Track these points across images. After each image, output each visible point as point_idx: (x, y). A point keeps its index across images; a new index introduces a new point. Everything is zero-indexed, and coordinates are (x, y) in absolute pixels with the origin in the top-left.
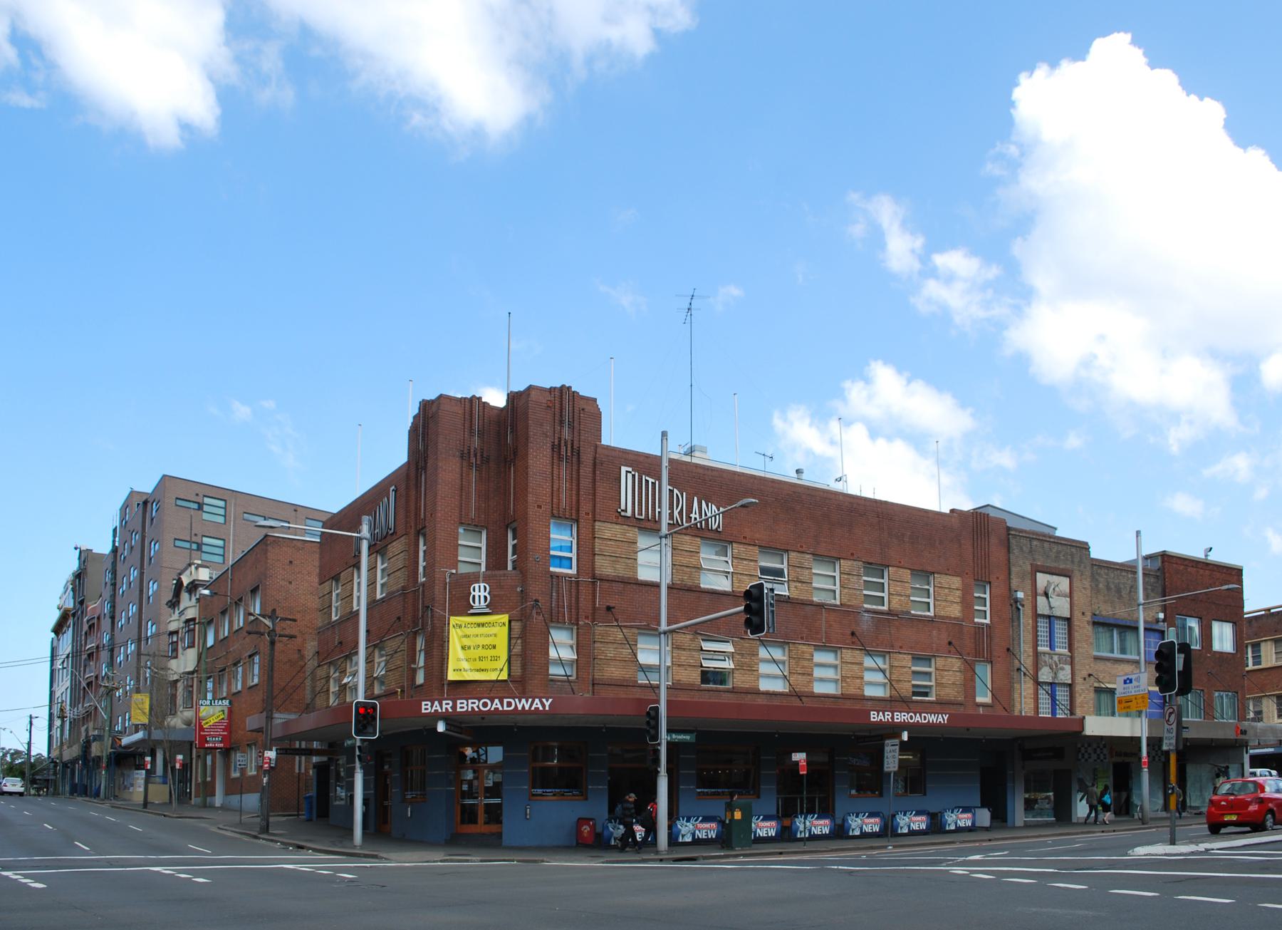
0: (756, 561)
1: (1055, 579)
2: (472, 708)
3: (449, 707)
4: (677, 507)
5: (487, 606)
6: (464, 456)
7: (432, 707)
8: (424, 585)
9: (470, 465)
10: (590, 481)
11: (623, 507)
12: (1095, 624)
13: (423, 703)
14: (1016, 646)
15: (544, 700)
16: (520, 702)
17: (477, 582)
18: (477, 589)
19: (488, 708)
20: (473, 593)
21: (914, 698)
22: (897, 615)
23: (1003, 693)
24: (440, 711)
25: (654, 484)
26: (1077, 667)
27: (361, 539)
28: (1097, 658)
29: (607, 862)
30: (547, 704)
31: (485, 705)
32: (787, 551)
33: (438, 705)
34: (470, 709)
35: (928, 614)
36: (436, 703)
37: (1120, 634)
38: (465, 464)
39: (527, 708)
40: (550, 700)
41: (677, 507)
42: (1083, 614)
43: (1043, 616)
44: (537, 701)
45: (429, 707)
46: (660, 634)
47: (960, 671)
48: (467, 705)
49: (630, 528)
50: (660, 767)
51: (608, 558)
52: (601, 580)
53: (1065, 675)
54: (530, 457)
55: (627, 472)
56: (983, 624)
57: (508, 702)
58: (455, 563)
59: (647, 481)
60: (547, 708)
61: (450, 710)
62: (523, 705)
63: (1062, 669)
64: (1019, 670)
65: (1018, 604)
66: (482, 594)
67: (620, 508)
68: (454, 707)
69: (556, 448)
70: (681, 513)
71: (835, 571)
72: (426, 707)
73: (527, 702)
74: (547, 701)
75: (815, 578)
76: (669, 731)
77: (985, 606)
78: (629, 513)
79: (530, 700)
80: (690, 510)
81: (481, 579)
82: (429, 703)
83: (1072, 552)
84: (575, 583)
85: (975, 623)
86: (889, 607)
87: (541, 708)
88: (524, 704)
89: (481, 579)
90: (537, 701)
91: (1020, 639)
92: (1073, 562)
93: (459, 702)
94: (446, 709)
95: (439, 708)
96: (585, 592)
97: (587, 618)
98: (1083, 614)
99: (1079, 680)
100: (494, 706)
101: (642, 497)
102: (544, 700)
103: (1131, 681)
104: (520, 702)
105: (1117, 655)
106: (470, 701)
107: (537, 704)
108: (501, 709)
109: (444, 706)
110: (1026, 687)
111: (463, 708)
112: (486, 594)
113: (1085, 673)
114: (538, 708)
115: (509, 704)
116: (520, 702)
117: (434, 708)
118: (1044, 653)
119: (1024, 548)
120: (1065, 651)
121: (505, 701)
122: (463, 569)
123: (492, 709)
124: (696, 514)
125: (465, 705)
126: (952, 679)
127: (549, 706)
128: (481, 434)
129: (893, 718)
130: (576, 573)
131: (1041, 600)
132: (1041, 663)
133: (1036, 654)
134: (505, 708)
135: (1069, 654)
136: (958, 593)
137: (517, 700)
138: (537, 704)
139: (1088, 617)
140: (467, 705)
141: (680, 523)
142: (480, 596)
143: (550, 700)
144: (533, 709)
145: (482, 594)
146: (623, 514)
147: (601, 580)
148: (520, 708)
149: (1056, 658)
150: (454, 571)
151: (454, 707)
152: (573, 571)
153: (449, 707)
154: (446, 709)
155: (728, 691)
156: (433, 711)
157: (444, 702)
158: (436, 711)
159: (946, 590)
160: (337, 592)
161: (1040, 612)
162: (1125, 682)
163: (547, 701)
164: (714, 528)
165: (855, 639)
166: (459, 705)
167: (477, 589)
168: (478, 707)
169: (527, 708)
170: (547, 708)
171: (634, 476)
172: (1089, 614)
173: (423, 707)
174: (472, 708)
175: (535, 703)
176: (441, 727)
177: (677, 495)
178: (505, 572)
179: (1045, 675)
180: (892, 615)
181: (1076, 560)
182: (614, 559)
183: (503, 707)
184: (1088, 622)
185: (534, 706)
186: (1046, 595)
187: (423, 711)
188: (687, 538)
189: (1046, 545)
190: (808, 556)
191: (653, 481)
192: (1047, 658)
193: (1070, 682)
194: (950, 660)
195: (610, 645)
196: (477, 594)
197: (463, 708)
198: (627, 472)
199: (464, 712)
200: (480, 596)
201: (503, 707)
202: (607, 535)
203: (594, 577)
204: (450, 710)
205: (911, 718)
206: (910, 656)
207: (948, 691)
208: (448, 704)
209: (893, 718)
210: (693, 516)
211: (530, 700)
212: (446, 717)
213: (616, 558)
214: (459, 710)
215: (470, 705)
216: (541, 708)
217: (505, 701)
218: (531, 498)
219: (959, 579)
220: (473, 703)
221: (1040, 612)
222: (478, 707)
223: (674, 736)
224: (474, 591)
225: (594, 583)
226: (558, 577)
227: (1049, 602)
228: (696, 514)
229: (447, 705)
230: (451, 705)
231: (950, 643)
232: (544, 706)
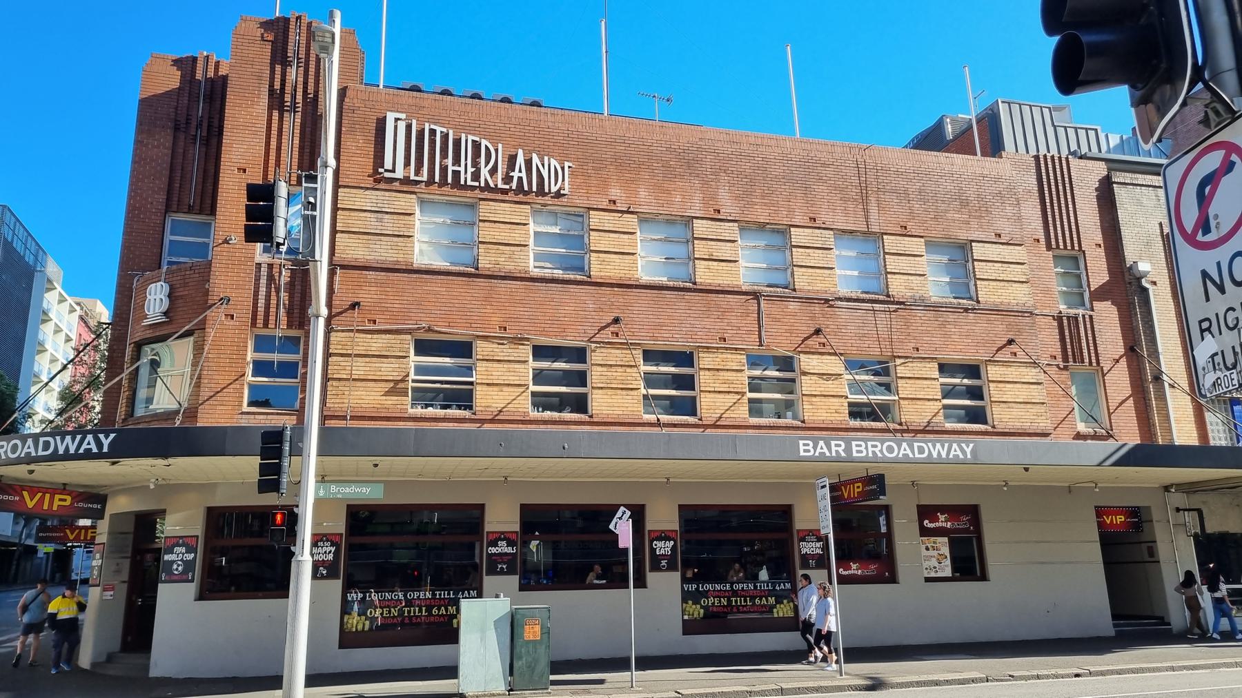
2: (874, 452)
3: (840, 449)
4: (487, 163)
7: (815, 448)
10: (1125, 239)
15: (101, 436)
16: (62, 442)
19: (894, 455)
30: (968, 451)
33: (32, 446)
36: (821, 443)
39: (944, 455)
41: (487, 163)
44: (90, 437)
45: (810, 448)
48: (866, 448)
50: (295, 545)
57: (44, 441)
59: (433, 132)
60: (969, 456)
61: (843, 454)
62: (939, 452)
65: (1143, 280)
67: (383, 167)
68: (848, 449)
73: (73, 440)
74: (107, 437)
79: (946, 445)
94: (837, 451)
95: (825, 450)
101: (435, 154)
102: (101, 436)
104: (62, 442)
106: (870, 444)
107: (89, 444)
108: (911, 456)
109: (834, 449)
114: (91, 449)
115: (921, 451)
116: (934, 447)
117: (819, 450)
124: (520, 171)
125: (863, 448)
127: (110, 445)
134: (917, 455)
138: (89, 444)
140: (866, 448)
141: (526, 188)
144: (951, 456)
145: (158, 297)
148: (935, 455)
151: (848, 449)
153: (840, 449)
156: (817, 454)
158: (822, 454)
163: (107, 437)
164: (554, 189)
166: (854, 449)
168: (881, 451)
169: (944, 455)
170: (969, 456)
171: (409, 127)
173: (802, 448)
174: (874, 452)
175: (953, 449)
177: (487, 147)
183: (914, 455)
185: (952, 453)
191: (445, 130)
197: (809, 451)
198: (397, 120)
199: (923, 458)
204: (843, 454)
208: (840, 446)
211: (946, 445)
215: (870, 449)
216: (961, 456)
220: (873, 446)
222: (881, 451)
224: (150, 295)
228: (520, 171)
230: (843, 446)
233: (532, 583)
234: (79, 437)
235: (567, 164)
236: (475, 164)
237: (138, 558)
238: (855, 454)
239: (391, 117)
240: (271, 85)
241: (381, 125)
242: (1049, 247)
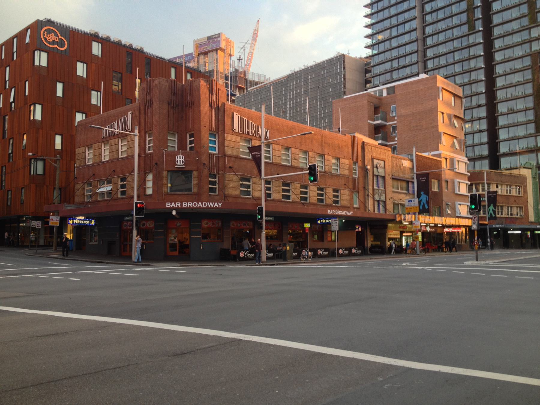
0: (280, 151)
1: (380, 162)
2: (189, 206)
5: (183, 165)
6: (169, 103)
7: (171, 205)
8: (151, 154)
9: (171, 107)
11: (235, 128)
12: (393, 179)
13: (167, 203)
14: (367, 186)
15: (219, 203)
17: (179, 155)
18: (179, 157)
20: (177, 159)
21: (241, 196)
22: (328, 173)
23: (364, 204)
24: (175, 206)
25: (245, 120)
26: (387, 195)
27: (135, 135)
28: (394, 192)
29: (246, 266)
30: (220, 205)
31: (195, 204)
32: (252, 139)
34: (188, 206)
35: (337, 173)
37: (400, 183)
38: (170, 106)
39: (212, 206)
40: (221, 203)
42: (389, 175)
43: (376, 175)
44: (216, 203)
45: (170, 205)
46: (262, 179)
47: (349, 195)
48: (187, 204)
49: (237, 137)
51: (230, 148)
52: (228, 156)
53: (383, 198)
54: (201, 106)
55: (236, 115)
56: (356, 178)
58: (167, 147)
59: (243, 119)
60: (220, 206)
61: (180, 206)
63: (382, 195)
64: (368, 195)
66: (181, 160)
68: (181, 205)
69: (210, 105)
70: (255, 132)
71: (289, 152)
72: (168, 205)
74: (220, 203)
75: (300, 158)
76: (266, 216)
77: (215, 144)
78: (237, 131)
79: (213, 203)
80: (258, 131)
81: (180, 154)
82: (170, 203)
83: (385, 152)
84: (218, 158)
85: (353, 177)
86: (272, 161)
87: (218, 206)
88: (211, 205)
89: (180, 154)
90: (216, 203)
91: (368, 183)
92: (385, 156)
93: (183, 203)
95: (174, 205)
96: (221, 160)
97: (222, 171)
98: (389, 175)
99: (388, 200)
100: (199, 205)
102: (219, 203)
103: (411, 201)
105: (399, 191)
106: (188, 203)
109: (177, 205)
110: (371, 201)
111: (169, 206)
112: (183, 160)
113: (390, 197)
115: (205, 205)
117: (172, 205)
118: (376, 189)
119: (369, 150)
120: (383, 189)
121: (204, 203)
122: (170, 149)
123: (198, 206)
125: (186, 204)
126: (346, 198)
127: (221, 205)
128: (176, 94)
129: (335, 212)
130: (217, 153)
131: (375, 169)
132: (375, 193)
133: (374, 189)
134: (204, 206)
135: (384, 190)
136: (348, 166)
137: (208, 203)
139: (390, 176)
140: (187, 204)
142: (180, 161)
143: (221, 203)
145: (181, 160)
146: (235, 131)
147: (228, 156)
148: (209, 206)
149: (380, 191)
150: (166, 150)
151: (181, 205)
152: (216, 152)
153: (179, 205)
154: (178, 206)
155: (271, 200)
157: (177, 203)
159: (344, 165)
160: (88, 152)
161: (375, 174)
162: (409, 202)
163: (220, 203)
165: (346, 186)
166: (183, 204)
167: (179, 157)
168: (192, 205)
169: (212, 206)
170: (220, 206)
171: (238, 116)
172: (391, 175)
173: (167, 205)
174: (189, 206)
176: (174, 213)
178: (186, 151)
179: (377, 197)
180: (326, 173)
181: (387, 155)
182: (232, 148)
183: (202, 205)
184: (391, 178)
185: (215, 205)
186: (377, 167)
187: (167, 206)
188: (257, 141)
189: (377, 149)
190: (298, 150)
192: (377, 191)
193: (385, 200)
194: (345, 191)
195: (230, 182)
196: (179, 159)
197: (169, 206)
200: (180, 161)
201: (202, 205)
202: (229, 139)
203: (225, 155)
204: (180, 206)
205: (341, 212)
206: (332, 189)
207: (345, 202)
209: (335, 212)
210: (259, 133)
212: (176, 209)
213: (232, 148)
214: (183, 206)
215: (189, 205)
216: (218, 206)
217: (204, 203)
218: (202, 123)
219: (348, 160)
221: (375, 174)
223: (267, 218)
225: (225, 158)
226: (212, 154)
227: (378, 171)
229: (178, 204)
230: (180, 204)
231: (345, 184)
232: (219, 205)
233: (529, 233)
234: (213, 203)
235: (269, 131)
236: (252, 129)
237: (269, 237)
238: (183, 206)
239: (235, 114)
240: (209, 101)
241: (233, 114)
242: (352, 160)
